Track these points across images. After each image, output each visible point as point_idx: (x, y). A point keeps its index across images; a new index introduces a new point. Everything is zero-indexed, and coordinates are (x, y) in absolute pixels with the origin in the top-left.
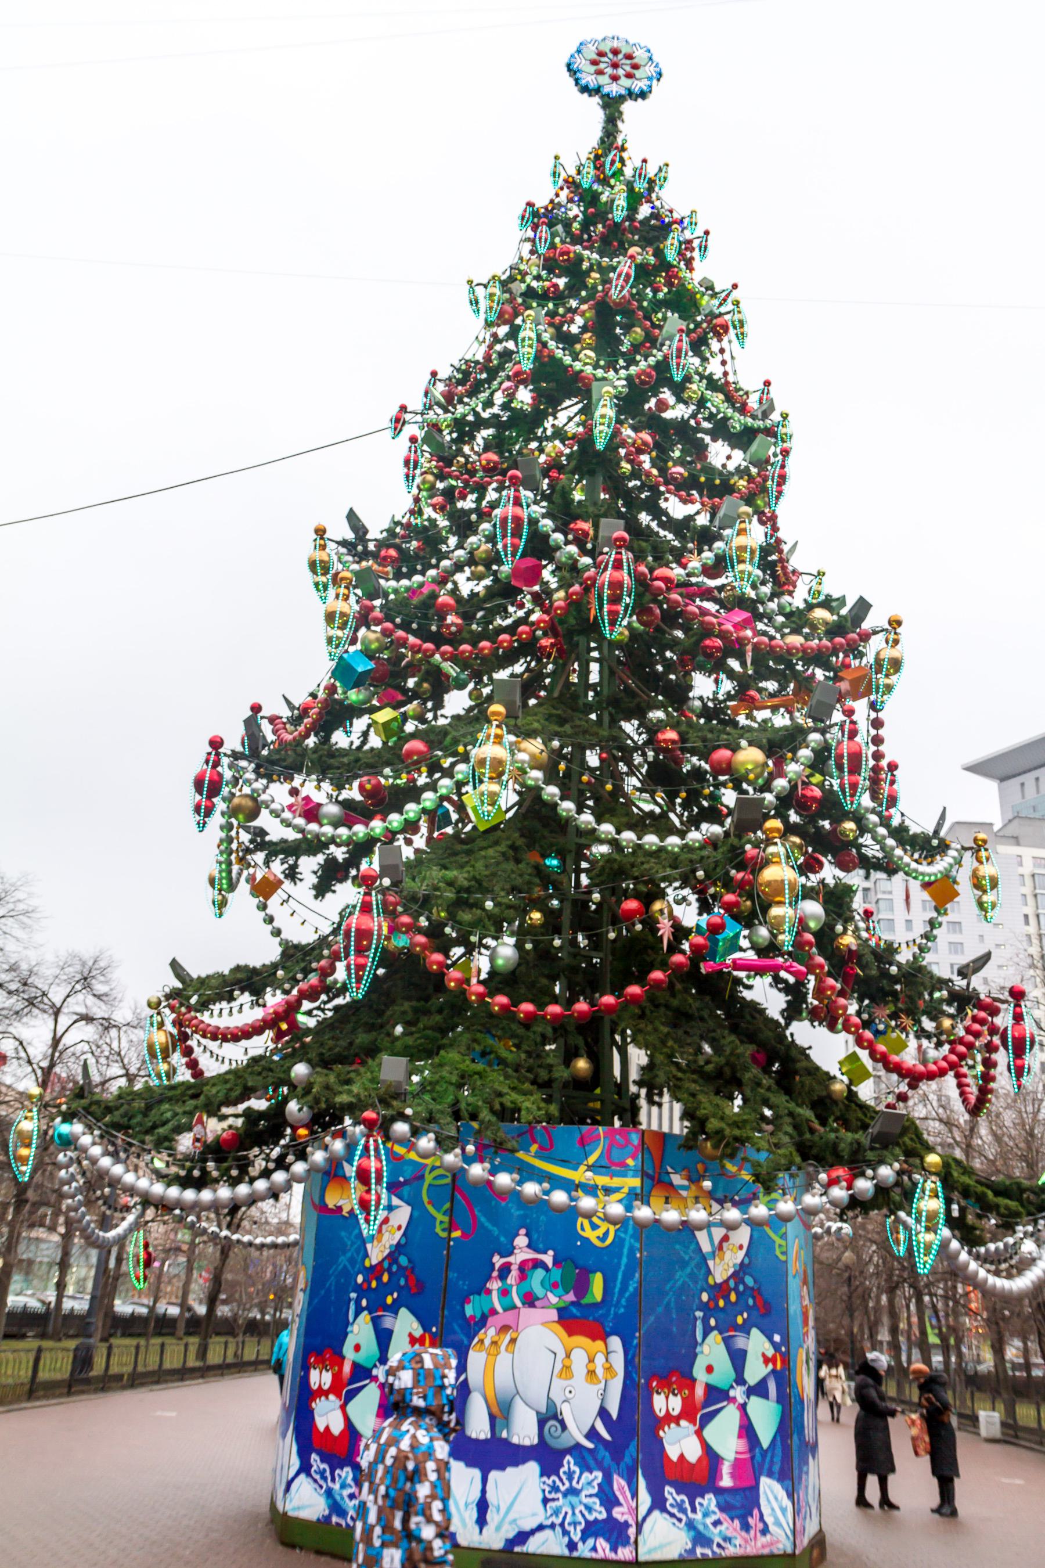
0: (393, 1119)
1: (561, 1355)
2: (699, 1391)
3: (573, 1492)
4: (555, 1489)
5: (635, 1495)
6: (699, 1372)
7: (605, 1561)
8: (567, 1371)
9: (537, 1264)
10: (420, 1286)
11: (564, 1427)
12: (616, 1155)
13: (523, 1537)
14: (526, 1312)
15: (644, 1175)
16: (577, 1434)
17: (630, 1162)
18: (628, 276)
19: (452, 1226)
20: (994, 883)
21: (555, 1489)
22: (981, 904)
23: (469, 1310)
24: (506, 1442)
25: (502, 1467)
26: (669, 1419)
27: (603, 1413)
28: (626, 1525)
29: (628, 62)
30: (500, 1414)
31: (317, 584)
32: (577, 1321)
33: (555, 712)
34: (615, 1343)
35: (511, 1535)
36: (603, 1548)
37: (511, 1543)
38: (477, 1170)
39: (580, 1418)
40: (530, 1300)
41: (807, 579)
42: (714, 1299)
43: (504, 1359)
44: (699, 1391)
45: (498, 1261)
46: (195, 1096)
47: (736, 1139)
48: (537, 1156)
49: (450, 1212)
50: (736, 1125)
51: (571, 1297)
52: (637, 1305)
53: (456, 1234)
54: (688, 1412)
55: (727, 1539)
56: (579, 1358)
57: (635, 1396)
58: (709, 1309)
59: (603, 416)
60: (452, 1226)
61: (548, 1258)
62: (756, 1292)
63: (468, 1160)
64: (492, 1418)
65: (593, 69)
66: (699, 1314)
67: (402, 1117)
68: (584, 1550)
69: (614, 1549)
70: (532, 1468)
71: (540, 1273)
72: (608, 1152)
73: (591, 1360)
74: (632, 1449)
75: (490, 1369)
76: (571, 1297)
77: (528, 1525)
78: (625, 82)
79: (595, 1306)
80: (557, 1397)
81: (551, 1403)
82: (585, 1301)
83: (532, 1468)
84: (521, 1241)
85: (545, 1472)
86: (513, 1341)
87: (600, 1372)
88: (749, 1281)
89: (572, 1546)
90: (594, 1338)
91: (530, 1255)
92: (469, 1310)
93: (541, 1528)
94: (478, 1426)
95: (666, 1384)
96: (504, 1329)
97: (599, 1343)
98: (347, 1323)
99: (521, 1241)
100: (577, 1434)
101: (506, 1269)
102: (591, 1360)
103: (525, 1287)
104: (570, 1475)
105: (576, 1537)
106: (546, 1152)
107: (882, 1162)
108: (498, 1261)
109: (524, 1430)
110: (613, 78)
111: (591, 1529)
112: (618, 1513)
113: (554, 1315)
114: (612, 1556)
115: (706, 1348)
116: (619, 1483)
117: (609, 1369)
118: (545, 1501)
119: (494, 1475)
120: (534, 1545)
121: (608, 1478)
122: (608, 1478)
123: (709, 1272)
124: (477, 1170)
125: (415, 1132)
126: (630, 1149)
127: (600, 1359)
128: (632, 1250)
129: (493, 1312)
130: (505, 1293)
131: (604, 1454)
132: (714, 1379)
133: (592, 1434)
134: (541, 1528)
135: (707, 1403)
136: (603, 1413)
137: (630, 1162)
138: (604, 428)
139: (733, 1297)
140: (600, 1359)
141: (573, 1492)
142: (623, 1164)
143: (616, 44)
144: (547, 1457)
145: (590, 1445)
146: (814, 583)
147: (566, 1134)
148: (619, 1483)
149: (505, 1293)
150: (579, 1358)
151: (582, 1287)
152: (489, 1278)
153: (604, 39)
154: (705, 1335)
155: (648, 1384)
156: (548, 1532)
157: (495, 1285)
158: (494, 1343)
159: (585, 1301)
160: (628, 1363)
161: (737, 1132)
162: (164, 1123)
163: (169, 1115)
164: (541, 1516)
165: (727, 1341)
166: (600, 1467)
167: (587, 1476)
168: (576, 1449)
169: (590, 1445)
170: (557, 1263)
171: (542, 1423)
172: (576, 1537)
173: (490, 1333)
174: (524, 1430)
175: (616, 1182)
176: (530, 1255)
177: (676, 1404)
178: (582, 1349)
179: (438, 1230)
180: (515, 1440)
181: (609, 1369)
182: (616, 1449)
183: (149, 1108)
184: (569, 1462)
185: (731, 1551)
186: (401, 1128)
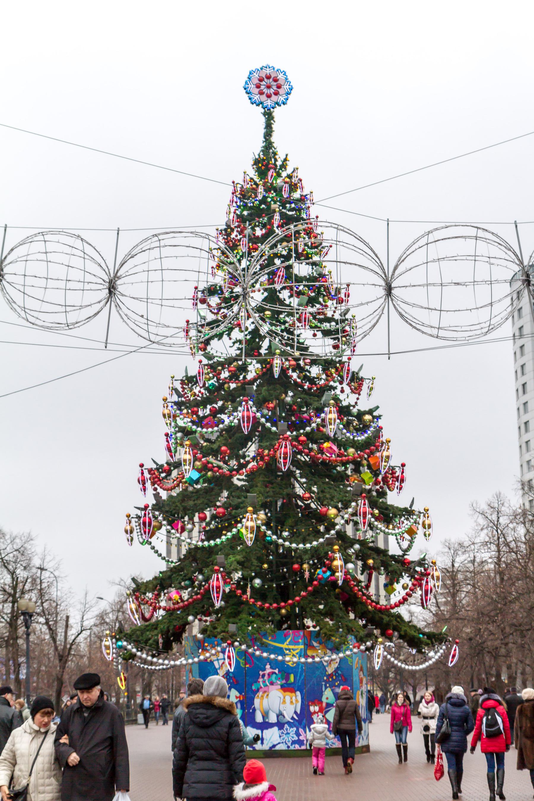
0: (234, 642)
1: (282, 697)
2: (324, 705)
3: (288, 733)
4: (283, 733)
5: (305, 732)
6: (324, 700)
7: (298, 750)
8: (284, 702)
9: (273, 673)
10: (237, 681)
11: (284, 717)
12: (296, 639)
13: (274, 746)
14: (271, 687)
15: (305, 644)
16: (288, 718)
17: (300, 641)
18: (283, 276)
19: (246, 664)
20: (430, 526)
21: (283, 733)
22: (425, 535)
23: (253, 688)
24: (268, 723)
25: (267, 729)
26: (315, 712)
27: (295, 712)
28: (303, 741)
29: (275, 84)
30: (265, 715)
31: (167, 424)
32: (286, 688)
33: (266, 479)
34: (298, 693)
35: (271, 745)
36: (297, 747)
37: (271, 748)
38: (258, 653)
39: (289, 714)
40: (272, 683)
41: (367, 381)
42: (328, 679)
43: (265, 701)
44: (324, 705)
45: (261, 673)
46: (156, 629)
47: (330, 635)
48: (271, 641)
49: (245, 659)
50: (330, 631)
51: (284, 681)
52: (304, 683)
53: (247, 666)
54: (321, 710)
55: (333, 743)
56: (288, 699)
57: (305, 707)
58: (327, 682)
59: (277, 364)
60: (246, 664)
61: (277, 671)
62: (342, 676)
63: (255, 650)
64: (263, 717)
65: (257, 91)
66: (323, 683)
67: (237, 641)
68: (292, 748)
69: (300, 747)
70: (276, 728)
71: (274, 675)
72: (293, 638)
73: (291, 698)
74: (304, 721)
75: (261, 703)
76: (284, 681)
77: (275, 743)
78: (274, 98)
79: (292, 684)
80: (282, 709)
81: (280, 711)
82: (289, 682)
83: (276, 728)
84: (268, 666)
85: (279, 729)
86: (268, 695)
87: (294, 702)
88: (340, 672)
89: (288, 747)
90: (292, 692)
91: (271, 670)
92: (253, 688)
93: (279, 743)
94: (259, 718)
95: (314, 704)
96: (265, 692)
97: (293, 694)
98: (322, 692)
99: (268, 666)
100: (288, 718)
101: (264, 676)
102: (291, 698)
103: (270, 680)
104: (287, 729)
105: (289, 744)
106: (274, 639)
107: (367, 641)
108: (261, 673)
109: (273, 719)
110: (268, 88)
111: (293, 742)
112: (301, 738)
113: (279, 687)
114: (299, 748)
115: (326, 693)
116: (301, 730)
117: (297, 701)
118: (280, 736)
119: (265, 731)
120: (277, 748)
121: (298, 729)
122: (298, 729)
123: (326, 671)
124: (258, 653)
125: (240, 645)
126: (300, 637)
127: (294, 698)
128: (302, 667)
129: (261, 687)
130: (264, 682)
131: (297, 723)
132: (328, 701)
133: (293, 718)
134: (279, 743)
135: (326, 708)
136: (295, 712)
137: (300, 641)
138: (278, 369)
139: (334, 677)
140: (294, 698)
141: (288, 733)
142: (298, 642)
143: (268, 71)
144: (280, 725)
145: (292, 721)
146: (370, 384)
147: (280, 634)
148: (301, 730)
149: (264, 682)
150: (288, 699)
151: (287, 678)
152: (259, 678)
153: (262, 69)
154: (326, 689)
155: (308, 703)
156: (281, 745)
157: (261, 680)
158: (262, 696)
159: (289, 682)
160: (302, 699)
161: (330, 633)
162: (150, 639)
163: (150, 636)
164: (279, 741)
165: (332, 690)
166: (295, 726)
167: (292, 729)
168: (288, 723)
169: (292, 721)
170: (279, 672)
171: (278, 716)
172: (289, 744)
173: (260, 694)
174: (273, 719)
175: (296, 647)
176: (271, 670)
177: (317, 708)
178: (288, 696)
179: (242, 665)
180: (270, 722)
181: (297, 701)
182: (300, 722)
183: (142, 634)
184: (286, 726)
185: (334, 746)
186: (236, 644)
